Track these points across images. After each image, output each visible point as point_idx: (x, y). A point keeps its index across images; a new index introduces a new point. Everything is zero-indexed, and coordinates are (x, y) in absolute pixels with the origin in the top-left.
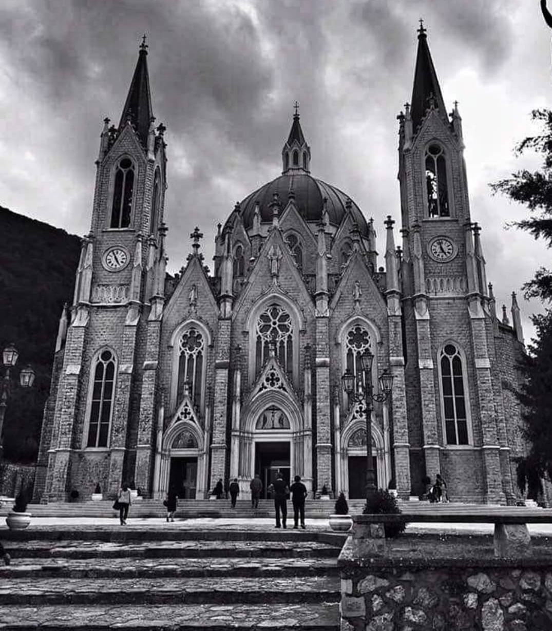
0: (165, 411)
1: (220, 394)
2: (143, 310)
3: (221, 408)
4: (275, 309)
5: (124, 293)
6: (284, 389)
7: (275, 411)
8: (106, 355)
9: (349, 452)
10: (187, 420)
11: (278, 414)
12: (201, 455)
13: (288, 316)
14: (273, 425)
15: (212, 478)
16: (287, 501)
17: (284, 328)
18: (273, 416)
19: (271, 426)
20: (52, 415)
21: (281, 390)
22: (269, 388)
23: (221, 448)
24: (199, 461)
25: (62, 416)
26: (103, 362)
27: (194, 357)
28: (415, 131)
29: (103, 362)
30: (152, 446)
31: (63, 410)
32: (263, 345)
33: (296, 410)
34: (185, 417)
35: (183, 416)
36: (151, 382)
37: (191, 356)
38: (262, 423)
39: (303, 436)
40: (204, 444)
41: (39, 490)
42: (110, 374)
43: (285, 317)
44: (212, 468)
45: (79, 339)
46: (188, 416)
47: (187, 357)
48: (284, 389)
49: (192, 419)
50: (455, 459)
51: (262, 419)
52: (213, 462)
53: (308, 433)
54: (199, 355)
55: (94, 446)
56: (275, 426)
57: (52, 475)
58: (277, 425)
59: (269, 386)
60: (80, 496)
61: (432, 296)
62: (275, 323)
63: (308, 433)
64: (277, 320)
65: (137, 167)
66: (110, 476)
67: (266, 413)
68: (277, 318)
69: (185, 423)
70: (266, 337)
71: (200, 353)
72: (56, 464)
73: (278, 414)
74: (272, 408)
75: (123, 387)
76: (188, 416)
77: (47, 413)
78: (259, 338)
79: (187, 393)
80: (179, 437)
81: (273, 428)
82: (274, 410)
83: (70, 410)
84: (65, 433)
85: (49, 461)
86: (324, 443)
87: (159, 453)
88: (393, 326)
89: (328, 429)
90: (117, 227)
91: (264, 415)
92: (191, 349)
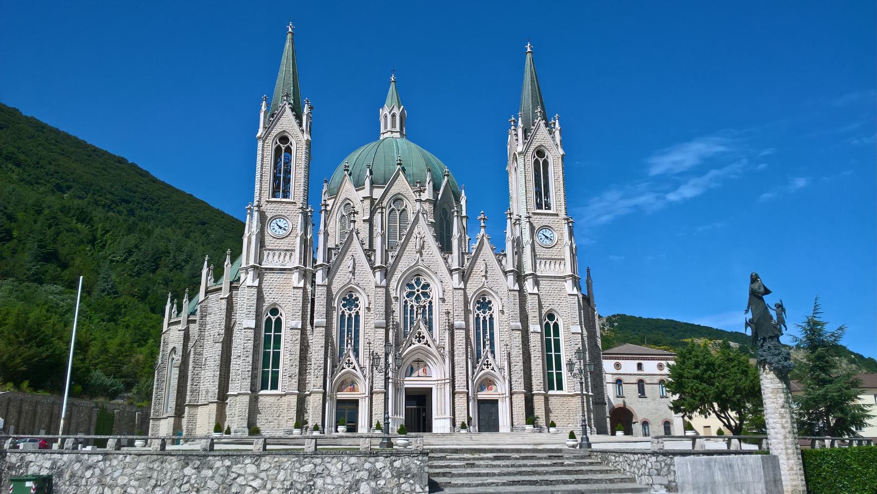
2: (308, 276)
4: (418, 279)
5: (288, 257)
6: (429, 346)
8: (274, 311)
13: (428, 285)
17: (425, 295)
23: (382, 393)
27: (353, 316)
32: (409, 308)
37: (350, 315)
40: (363, 388)
42: (278, 328)
43: (426, 286)
47: (482, 319)
48: (429, 346)
50: (102, 403)
54: (491, 318)
55: (553, 389)
61: (538, 274)
62: (418, 291)
65: (294, 143)
69: (348, 372)
71: (357, 313)
78: (406, 302)
90: (541, 208)
92: (350, 309)
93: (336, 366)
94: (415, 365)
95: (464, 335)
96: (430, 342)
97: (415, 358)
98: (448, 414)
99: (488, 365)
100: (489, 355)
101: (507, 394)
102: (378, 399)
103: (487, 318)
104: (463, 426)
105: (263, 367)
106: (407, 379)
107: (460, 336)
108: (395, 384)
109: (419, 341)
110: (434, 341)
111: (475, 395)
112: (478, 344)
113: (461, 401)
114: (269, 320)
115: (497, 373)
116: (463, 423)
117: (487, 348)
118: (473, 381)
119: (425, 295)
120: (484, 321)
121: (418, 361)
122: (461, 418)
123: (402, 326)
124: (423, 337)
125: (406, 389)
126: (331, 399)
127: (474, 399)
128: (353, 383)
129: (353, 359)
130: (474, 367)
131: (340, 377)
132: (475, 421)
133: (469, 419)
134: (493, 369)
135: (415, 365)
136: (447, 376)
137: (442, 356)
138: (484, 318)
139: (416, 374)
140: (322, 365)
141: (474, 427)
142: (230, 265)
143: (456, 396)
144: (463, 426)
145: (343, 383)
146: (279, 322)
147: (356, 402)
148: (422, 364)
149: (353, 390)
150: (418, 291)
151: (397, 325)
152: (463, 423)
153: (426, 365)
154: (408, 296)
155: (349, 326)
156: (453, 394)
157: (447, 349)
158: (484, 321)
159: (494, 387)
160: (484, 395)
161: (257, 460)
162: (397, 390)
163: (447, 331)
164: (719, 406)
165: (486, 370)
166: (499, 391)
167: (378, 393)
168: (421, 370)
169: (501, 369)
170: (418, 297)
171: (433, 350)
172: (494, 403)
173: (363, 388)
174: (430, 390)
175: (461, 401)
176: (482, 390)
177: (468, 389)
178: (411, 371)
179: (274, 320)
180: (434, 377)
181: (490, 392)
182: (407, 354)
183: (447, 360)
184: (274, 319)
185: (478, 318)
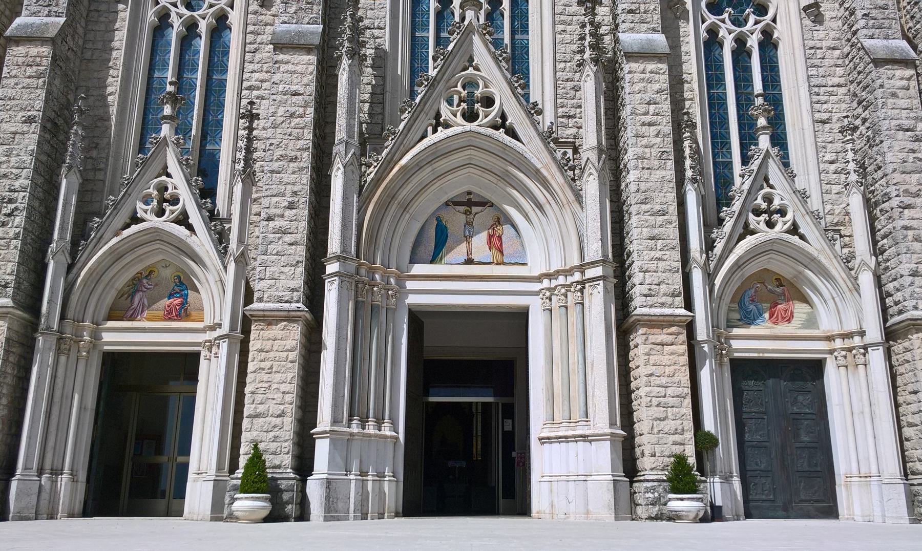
7: (475, 209)
9: (735, 344)
10: (165, 224)
12: (211, 345)
15: (245, 423)
16: (682, 24)
21: (501, 134)
22: (460, 126)
23: (289, 318)
24: (203, 364)
27: (203, 27)
30: (18, 304)
34: (160, 213)
36: (34, 82)
37: (191, 27)
39: (583, 283)
40: (215, 300)
44: (247, 390)
46: (168, 208)
49: (183, 220)
51: (432, 232)
52: (251, 367)
53: (591, 273)
54: (768, 44)
56: (475, 257)
59: (459, 119)
63: (598, 271)
69: (156, 235)
76: (168, 208)
79: (166, 130)
82: (470, 203)
86: (663, 305)
91: (439, 220)
94: (455, 220)
95: (663, 81)
96: (516, 117)
97: (456, 186)
98: (601, 419)
99: (772, 214)
100: (774, 172)
101: (874, 333)
102: (276, 348)
103: (753, 42)
104: (682, 479)
105: (246, 305)
106: (418, 269)
107: (643, 86)
108: (358, 288)
109: (470, 116)
110: (533, 111)
111: (720, 341)
112: (720, 140)
113: (659, 363)
115: (815, 245)
116: (680, 460)
117: (764, 141)
118: (709, 277)
120: (741, 52)
121: (469, 203)
122: (664, 437)
123: (402, 67)
124: (488, 102)
125: (419, 320)
126: (61, 344)
127: (719, 356)
128: (183, 285)
129: (179, 183)
130: (711, 223)
131: (116, 255)
132: (727, 453)
133: (705, 443)
134: (794, 230)
135: (455, 220)
136: (594, 251)
137: (570, 169)
138: (740, 41)
139: (460, 252)
140: (304, 199)
141: (727, 479)
143: (638, 338)
144: (682, 479)
145: (136, 284)
147: (185, 365)
148: (483, 216)
149: (182, 312)
151: (381, 60)
152: (680, 460)
153: (503, 219)
155: (184, 65)
156: (624, 326)
157: (590, 138)
158: (741, 52)
159: (800, 309)
160: (756, 340)
161: (842, 224)
162: (365, 312)
163: (590, 70)
165: (764, 234)
166: (827, 323)
167: (269, 319)
168: (480, 241)
169: (834, 232)
171: (532, 148)
173: (215, 300)
174: (308, 520)
175: (659, 363)
176: (748, 319)
177: (689, 305)
178: (436, 243)
180: (535, 262)
181: (783, 329)
182: (417, 165)
183: (591, 186)
185: (712, 42)
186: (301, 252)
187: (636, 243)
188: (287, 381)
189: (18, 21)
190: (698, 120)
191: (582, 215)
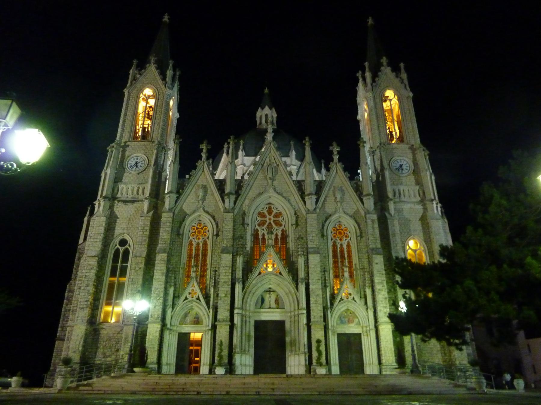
0: (175, 291)
1: (225, 277)
3: (224, 290)
7: (271, 293)
11: (273, 296)
14: (270, 305)
17: (278, 224)
18: (270, 297)
19: (268, 307)
20: (72, 297)
25: (81, 294)
26: (120, 248)
28: (374, 81)
29: (120, 248)
31: (82, 288)
33: (290, 292)
35: (190, 295)
37: (198, 244)
38: (260, 303)
41: (57, 361)
42: (126, 258)
45: (100, 228)
48: (184, 300)
51: (260, 300)
56: (272, 306)
57: (68, 347)
58: (273, 305)
60: (387, 315)
62: (270, 219)
64: (268, 221)
66: (122, 349)
67: (264, 294)
68: (272, 215)
70: (263, 230)
72: (72, 338)
73: (273, 296)
74: (268, 290)
75: (137, 269)
77: (68, 295)
80: (186, 315)
81: (270, 308)
82: (270, 291)
83: (88, 288)
84: (82, 309)
85: (67, 335)
87: (168, 329)
88: (371, 223)
89: (320, 308)
91: (262, 296)
93: (179, 297)
97: (266, 287)
103: (345, 246)
114: (117, 251)
119: (278, 224)
140: (229, 292)
142: (223, 341)
146: (126, 253)
150: (270, 219)
154: (259, 225)
164: (457, 339)
170: (270, 226)
172: (124, 284)
179: (121, 251)
184: (122, 249)
186: (228, 308)
187: (312, 305)
188: (268, 314)
189: (158, 248)
190: (367, 154)
191: (298, 294)
